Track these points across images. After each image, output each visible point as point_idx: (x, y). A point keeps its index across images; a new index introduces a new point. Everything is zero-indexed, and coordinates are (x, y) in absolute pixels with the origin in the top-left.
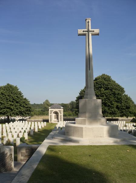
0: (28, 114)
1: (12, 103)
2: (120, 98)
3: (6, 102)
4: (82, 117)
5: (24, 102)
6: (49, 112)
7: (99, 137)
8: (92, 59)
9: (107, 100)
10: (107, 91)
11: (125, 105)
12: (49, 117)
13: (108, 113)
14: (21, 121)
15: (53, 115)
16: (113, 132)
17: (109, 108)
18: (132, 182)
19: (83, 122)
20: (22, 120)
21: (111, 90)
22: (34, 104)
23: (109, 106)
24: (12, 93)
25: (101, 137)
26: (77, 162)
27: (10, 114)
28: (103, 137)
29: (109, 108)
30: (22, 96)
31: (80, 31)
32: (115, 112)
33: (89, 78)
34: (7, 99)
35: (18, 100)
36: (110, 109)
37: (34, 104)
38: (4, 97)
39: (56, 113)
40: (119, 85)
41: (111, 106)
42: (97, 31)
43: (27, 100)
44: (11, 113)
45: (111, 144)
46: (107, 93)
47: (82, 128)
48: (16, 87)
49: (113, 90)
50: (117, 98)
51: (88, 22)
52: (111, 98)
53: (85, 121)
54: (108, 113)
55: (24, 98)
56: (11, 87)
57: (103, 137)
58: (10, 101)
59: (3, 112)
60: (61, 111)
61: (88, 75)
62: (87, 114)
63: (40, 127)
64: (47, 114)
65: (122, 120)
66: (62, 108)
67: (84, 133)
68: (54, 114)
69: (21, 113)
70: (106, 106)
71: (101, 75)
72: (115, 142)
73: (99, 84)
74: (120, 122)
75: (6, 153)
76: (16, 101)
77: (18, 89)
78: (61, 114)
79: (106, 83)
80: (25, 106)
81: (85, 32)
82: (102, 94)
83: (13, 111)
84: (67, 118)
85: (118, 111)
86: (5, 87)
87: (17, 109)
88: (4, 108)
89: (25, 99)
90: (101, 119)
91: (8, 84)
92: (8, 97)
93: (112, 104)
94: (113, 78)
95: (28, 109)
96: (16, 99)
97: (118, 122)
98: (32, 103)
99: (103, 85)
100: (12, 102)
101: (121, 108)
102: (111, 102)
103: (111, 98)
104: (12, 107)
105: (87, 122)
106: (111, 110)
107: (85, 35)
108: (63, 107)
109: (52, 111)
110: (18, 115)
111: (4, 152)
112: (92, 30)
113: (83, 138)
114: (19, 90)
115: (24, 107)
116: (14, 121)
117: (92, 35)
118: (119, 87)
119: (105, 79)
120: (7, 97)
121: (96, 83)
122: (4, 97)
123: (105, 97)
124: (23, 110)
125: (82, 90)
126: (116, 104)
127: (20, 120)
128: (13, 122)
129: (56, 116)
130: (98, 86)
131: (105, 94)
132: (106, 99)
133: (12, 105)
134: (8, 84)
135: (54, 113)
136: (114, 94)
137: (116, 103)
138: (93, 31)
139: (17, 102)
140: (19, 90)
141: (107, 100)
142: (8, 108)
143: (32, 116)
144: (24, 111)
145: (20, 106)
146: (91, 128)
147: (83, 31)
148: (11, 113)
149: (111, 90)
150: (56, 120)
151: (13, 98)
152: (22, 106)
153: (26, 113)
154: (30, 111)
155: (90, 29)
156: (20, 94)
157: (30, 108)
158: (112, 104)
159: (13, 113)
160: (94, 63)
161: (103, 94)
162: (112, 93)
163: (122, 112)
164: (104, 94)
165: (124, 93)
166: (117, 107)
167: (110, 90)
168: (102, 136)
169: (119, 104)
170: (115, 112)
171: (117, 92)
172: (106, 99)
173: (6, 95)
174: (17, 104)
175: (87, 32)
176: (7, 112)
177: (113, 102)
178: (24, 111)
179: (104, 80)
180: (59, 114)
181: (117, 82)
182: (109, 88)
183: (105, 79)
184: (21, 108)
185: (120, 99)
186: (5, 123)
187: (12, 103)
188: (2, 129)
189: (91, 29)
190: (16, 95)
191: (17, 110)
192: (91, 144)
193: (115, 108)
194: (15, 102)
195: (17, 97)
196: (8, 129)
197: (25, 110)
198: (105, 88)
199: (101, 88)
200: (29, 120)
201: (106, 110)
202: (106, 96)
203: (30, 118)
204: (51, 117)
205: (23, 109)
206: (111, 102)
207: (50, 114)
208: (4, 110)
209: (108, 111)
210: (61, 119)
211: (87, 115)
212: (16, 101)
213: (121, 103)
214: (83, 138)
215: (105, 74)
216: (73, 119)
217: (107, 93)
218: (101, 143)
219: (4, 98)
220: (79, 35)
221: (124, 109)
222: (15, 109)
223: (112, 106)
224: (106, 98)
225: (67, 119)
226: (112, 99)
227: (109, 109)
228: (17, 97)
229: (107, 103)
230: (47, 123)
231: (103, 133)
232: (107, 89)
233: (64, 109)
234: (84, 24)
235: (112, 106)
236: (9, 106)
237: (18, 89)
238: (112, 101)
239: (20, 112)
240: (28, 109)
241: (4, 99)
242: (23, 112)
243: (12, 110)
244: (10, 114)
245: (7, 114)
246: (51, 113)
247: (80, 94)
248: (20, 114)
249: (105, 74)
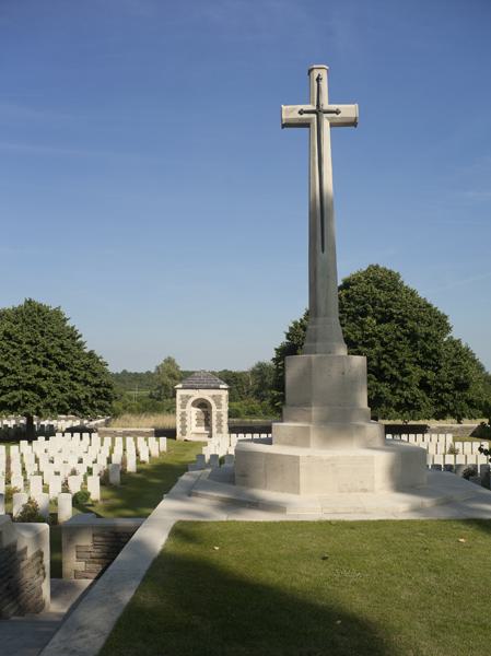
0: (101, 408)
1: (45, 371)
2: (434, 351)
3: (22, 364)
4: (296, 421)
5: (87, 367)
6: (179, 402)
7: (356, 491)
8: (331, 211)
9: (385, 359)
10: (385, 326)
11: (451, 375)
12: (178, 418)
13: (389, 404)
14: (77, 435)
15: (193, 413)
16: (409, 474)
17: (393, 386)
18: (475, 653)
19: (301, 439)
20: (81, 430)
21: (402, 323)
22: (125, 371)
23: (393, 379)
24: (42, 333)
25: (365, 490)
26: (276, 580)
27: (38, 408)
28: (373, 491)
29: (393, 386)
30: (80, 346)
31: (290, 112)
32: (414, 401)
33: (320, 280)
34: (26, 356)
35: (63, 360)
36: (398, 391)
37: (125, 371)
38: (14, 347)
39: (203, 405)
40: (429, 306)
41: (400, 378)
42: (349, 111)
43: (96, 359)
44: (41, 405)
45: (401, 518)
46: (386, 334)
47: (296, 459)
48: (57, 313)
49: (410, 324)
50: (424, 350)
51: (318, 79)
52: (401, 350)
53: (308, 434)
54: (389, 404)
55: (86, 351)
56: (39, 311)
57: (373, 491)
58: (36, 361)
59: (12, 403)
60: (220, 399)
61: (319, 270)
62: (313, 408)
63: (144, 457)
64: (171, 410)
65: (442, 431)
66: (225, 386)
67: (303, 478)
68: (195, 410)
69: (76, 407)
70: (384, 380)
71: (365, 269)
72: (415, 509)
73: (358, 303)
74: (434, 436)
75: (20, 547)
76: (56, 362)
77: (65, 320)
78: (221, 410)
79: (383, 296)
80: (89, 379)
81: (305, 116)
82: (367, 336)
83: (48, 399)
84: (241, 422)
85: (427, 399)
86: (17, 312)
87: (62, 391)
88: (16, 388)
89: (91, 355)
90: (363, 427)
91: (29, 302)
92: (29, 349)
93: (405, 374)
94: (409, 280)
95: (101, 390)
96: (58, 355)
97: (427, 436)
98: (114, 368)
99: (373, 305)
100: (45, 364)
101: (438, 388)
102: (401, 367)
103: (401, 350)
104: (43, 385)
105: (314, 437)
106: (401, 395)
107: (306, 125)
108: (227, 382)
109: (188, 397)
110: (65, 413)
111: (15, 546)
112: (334, 107)
113: (298, 493)
114: (69, 324)
115: (87, 383)
116: (49, 433)
117: (332, 125)
118: (430, 313)
119: (378, 284)
120: (25, 346)
121: (347, 296)
122: (14, 347)
123: (379, 348)
124: (82, 396)
125: (295, 323)
126: (417, 373)
127: (72, 430)
128: (47, 439)
129: (203, 417)
130: (353, 309)
131: (380, 338)
132: (384, 356)
133: (45, 377)
134: (29, 302)
135: (193, 404)
136: (413, 336)
137: (418, 368)
138: (337, 112)
139: (62, 367)
140: (69, 324)
141: (385, 359)
142: (28, 387)
143: (116, 415)
144: (87, 396)
145: (73, 379)
146: (328, 460)
147: (301, 112)
148: (41, 405)
149: (402, 323)
150: (202, 429)
151: (46, 350)
152: (78, 381)
153: (92, 406)
154: (108, 397)
155: (326, 105)
156: (73, 336)
157: (109, 387)
158: (405, 374)
159: (48, 406)
160: (339, 227)
161: (370, 335)
162: (405, 334)
163: (442, 402)
164: (376, 336)
165: (447, 332)
166: (424, 385)
167: (398, 321)
168: (367, 486)
169: (430, 375)
170: (414, 401)
171: (421, 330)
172: (384, 356)
173: (20, 342)
174: (60, 373)
175: (314, 116)
176: (27, 402)
177: (409, 367)
178: (87, 396)
179: (377, 287)
180: (214, 410)
181: (421, 294)
182: (392, 314)
183: (379, 282)
184: (74, 389)
185: (435, 356)
186: (17, 442)
187: (45, 371)
188: (8, 461)
189: (330, 103)
190: (58, 342)
191: (60, 396)
192: (328, 518)
193: (415, 389)
194: (55, 365)
195: (62, 346)
196: (29, 461)
197: (89, 395)
198: (379, 316)
199: (364, 314)
200: (104, 429)
201: (381, 393)
202: (383, 344)
203: (107, 424)
204: (183, 420)
205: (82, 392)
206: (401, 367)
207: (179, 410)
208: (15, 393)
209: (390, 397)
210: (219, 425)
211: (315, 411)
212: (56, 362)
213: (437, 368)
214: (298, 493)
215: (377, 266)
216: (263, 427)
217: (386, 334)
218: (365, 513)
219: (15, 351)
220: (284, 126)
221: (447, 391)
222: (56, 392)
223: (405, 379)
224: (384, 353)
225: (241, 427)
226: (405, 353)
227: (393, 391)
228: (62, 346)
229: (385, 368)
230: (171, 440)
231: (373, 477)
232: (385, 318)
233: (230, 390)
234: (302, 86)
235: (405, 379)
236: (34, 381)
237: (65, 320)
238: (404, 361)
239: (71, 400)
240: (101, 390)
241: (15, 354)
242: (83, 403)
243: (43, 394)
244: (38, 408)
245: (24, 407)
246: (183, 406)
247: (288, 336)
248: (72, 407)
249: (377, 266)
